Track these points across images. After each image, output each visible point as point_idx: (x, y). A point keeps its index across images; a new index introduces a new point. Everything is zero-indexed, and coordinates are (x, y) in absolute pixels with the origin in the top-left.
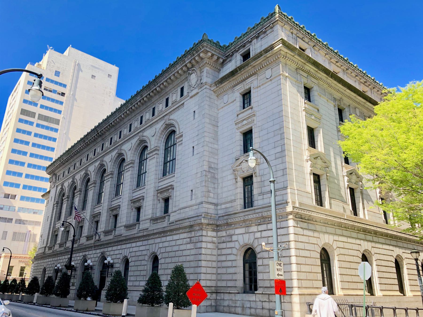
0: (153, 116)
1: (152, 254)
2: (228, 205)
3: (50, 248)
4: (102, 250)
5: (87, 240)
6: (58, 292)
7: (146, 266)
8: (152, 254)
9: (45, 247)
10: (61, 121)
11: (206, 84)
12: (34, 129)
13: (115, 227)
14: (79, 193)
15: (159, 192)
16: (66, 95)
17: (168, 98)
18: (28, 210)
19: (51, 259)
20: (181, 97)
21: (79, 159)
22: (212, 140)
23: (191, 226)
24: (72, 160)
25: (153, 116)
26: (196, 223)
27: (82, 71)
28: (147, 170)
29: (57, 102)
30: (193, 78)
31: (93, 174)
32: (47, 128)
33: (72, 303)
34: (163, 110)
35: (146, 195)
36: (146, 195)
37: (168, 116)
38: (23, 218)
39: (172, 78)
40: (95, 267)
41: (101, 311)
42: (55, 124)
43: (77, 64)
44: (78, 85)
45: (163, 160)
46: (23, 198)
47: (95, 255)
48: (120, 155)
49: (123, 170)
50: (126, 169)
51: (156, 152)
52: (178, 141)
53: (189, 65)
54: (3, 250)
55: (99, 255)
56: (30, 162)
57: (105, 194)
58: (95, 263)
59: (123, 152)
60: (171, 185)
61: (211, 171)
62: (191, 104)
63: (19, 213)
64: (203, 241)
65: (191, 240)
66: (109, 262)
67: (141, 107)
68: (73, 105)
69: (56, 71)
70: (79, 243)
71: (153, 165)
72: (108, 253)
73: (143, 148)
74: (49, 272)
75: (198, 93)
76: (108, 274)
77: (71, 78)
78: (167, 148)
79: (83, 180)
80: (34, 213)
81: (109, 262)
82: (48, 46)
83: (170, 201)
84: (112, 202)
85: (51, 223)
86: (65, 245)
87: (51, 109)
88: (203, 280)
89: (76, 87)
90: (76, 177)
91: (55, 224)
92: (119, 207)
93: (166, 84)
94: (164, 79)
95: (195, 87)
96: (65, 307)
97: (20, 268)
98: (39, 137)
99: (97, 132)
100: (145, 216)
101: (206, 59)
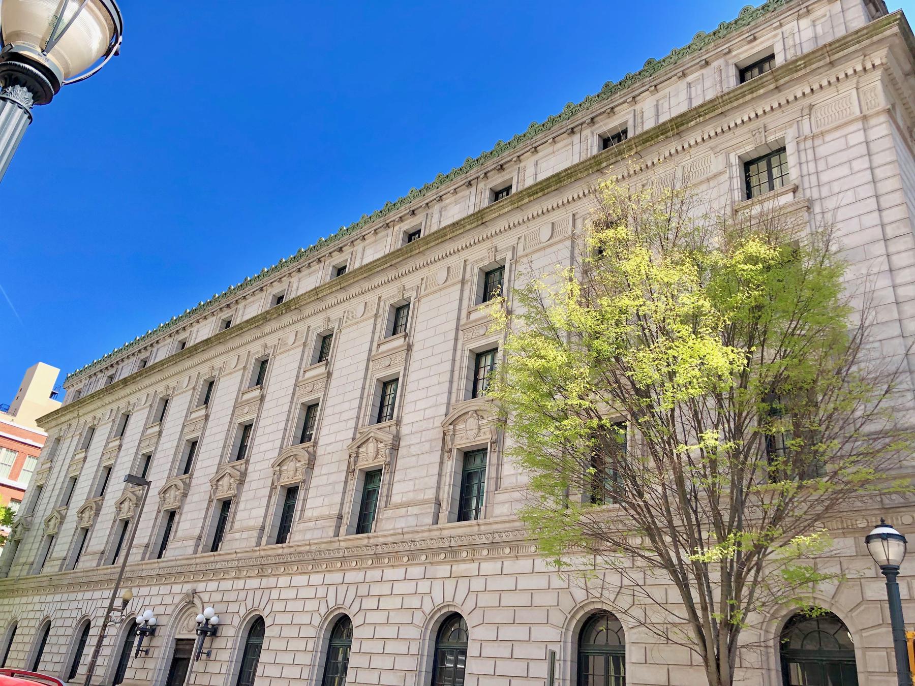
4: (188, 588)
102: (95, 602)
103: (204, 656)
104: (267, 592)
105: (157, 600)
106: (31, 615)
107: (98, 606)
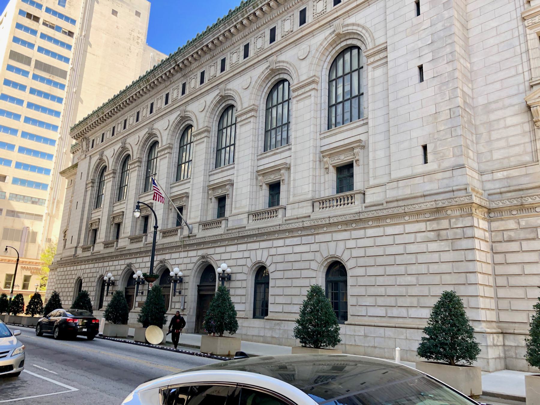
1: (255, 265)
2: (514, 173)
3: (85, 249)
4: (128, 261)
8: (326, 260)
9: (76, 247)
10: (68, 73)
12: (28, 82)
13: (117, 238)
15: (328, 155)
16: (75, 36)
17: (305, 9)
18: (24, 198)
20: (301, 24)
22: (463, 51)
23: (438, 210)
24: (119, 114)
26: (454, 203)
28: (157, 172)
29: (63, 44)
31: (135, 148)
32: (49, 82)
33: (131, 332)
35: (237, 179)
36: (237, 179)
37: (275, 56)
38: (17, 209)
39: (220, 39)
40: (186, 279)
46: (16, 181)
47: (186, 260)
48: (151, 135)
52: (239, 120)
54: (6, 249)
56: (26, 130)
58: (187, 273)
59: (155, 131)
60: (230, 180)
61: (467, 110)
63: (11, 202)
64: (476, 236)
65: (439, 235)
68: (85, 51)
70: (117, 246)
71: (201, 152)
72: (137, 266)
73: (185, 128)
77: (81, 10)
78: (222, 130)
79: (119, 156)
80: (33, 203)
81: (224, 271)
83: (228, 201)
87: (54, 55)
88: (482, 309)
91: (90, 214)
92: (187, 196)
96: (122, 338)
97: (23, 277)
98: (37, 95)
99: (176, 62)
105: (112, 268)
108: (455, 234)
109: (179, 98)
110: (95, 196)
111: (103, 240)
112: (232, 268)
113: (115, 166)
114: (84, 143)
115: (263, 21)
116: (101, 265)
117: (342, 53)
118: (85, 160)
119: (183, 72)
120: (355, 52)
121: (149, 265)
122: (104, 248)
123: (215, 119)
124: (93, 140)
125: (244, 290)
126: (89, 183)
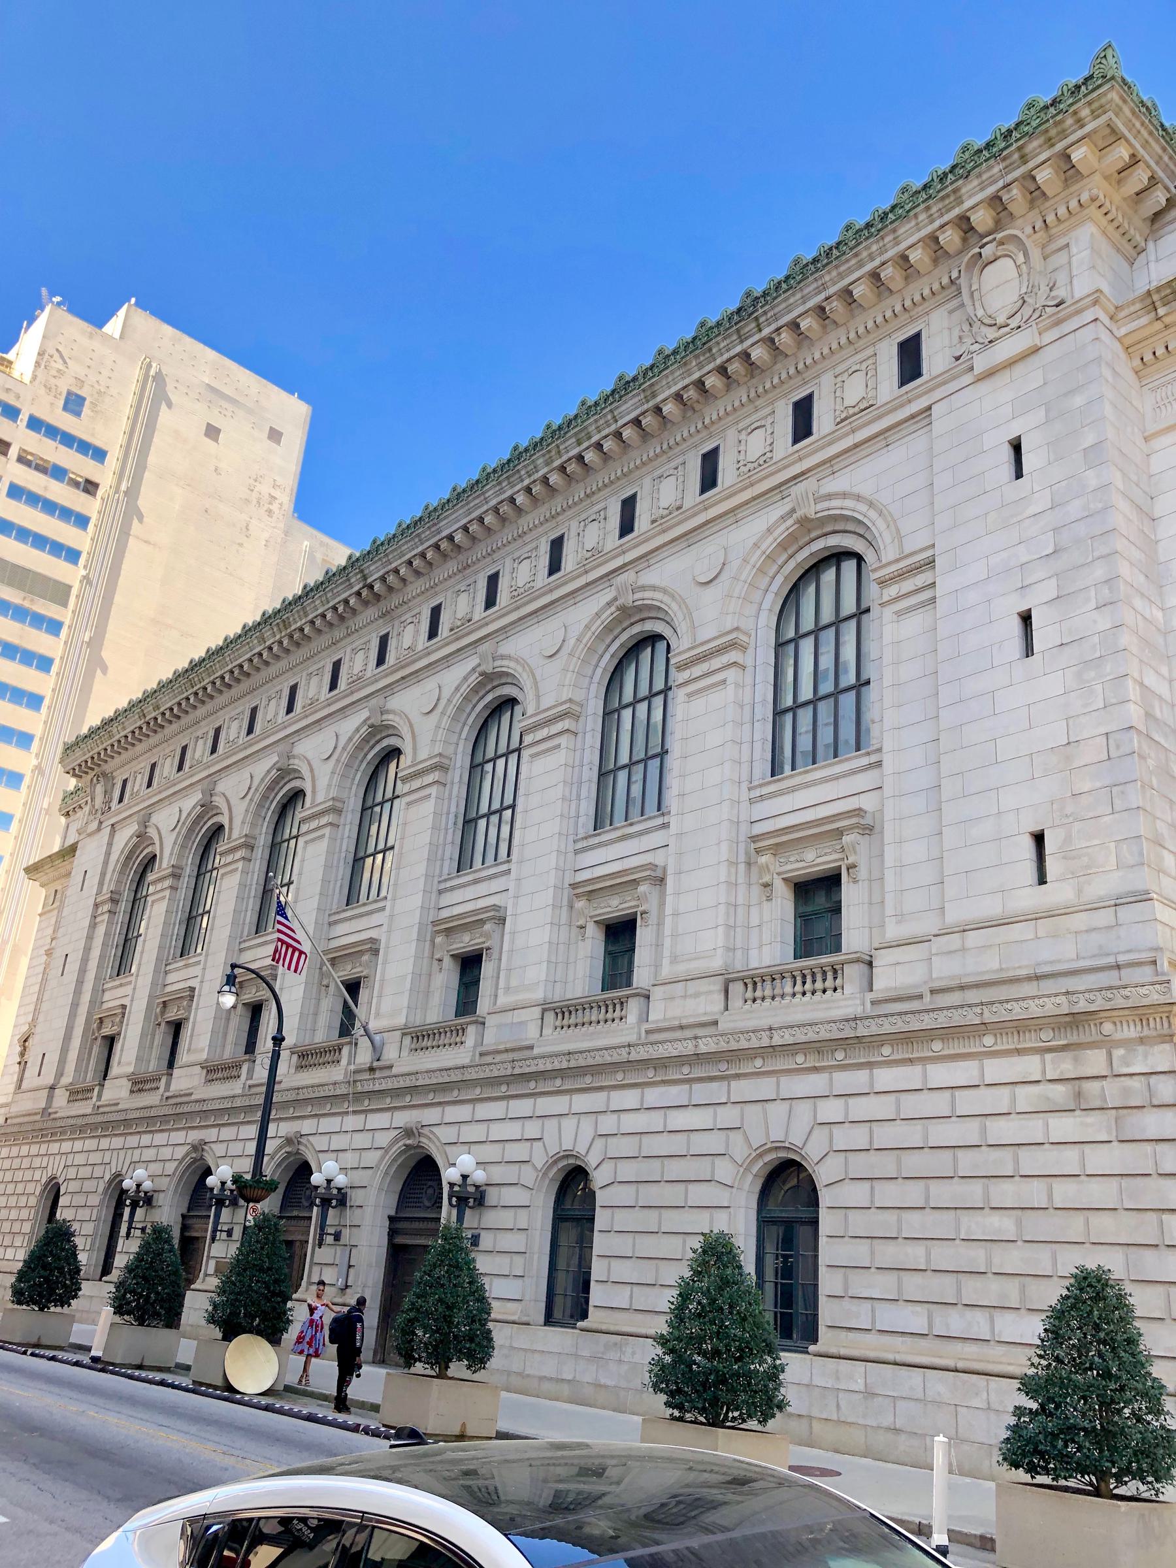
0: (331, 689)
3: (77, 1093)
4: (194, 1136)
5: (300, 1067)
6: (420, 1333)
7: (523, 1213)
8: (760, 1155)
9: (52, 1088)
10: (74, 592)
11: (1096, 302)
14: (167, 883)
15: (769, 848)
19: (91, 1144)
21: (245, 707)
22: (1142, 578)
23: (1075, 1020)
24: (201, 711)
25: (331, 689)
26: (1120, 1002)
27: (170, 405)
28: (869, 672)
29: (66, 514)
30: (1000, 284)
33: (185, 1350)
34: (369, 674)
35: (515, 905)
41: (375, 1408)
42: (53, 600)
43: (152, 373)
44: (152, 459)
45: (352, 849)
49: (216, 865)
50: (225, 865)
51: (733, 656)
52: (528, 739)
53: (982, 219)
55: (180, 1152)
57: (298, 889)
59: (296, 763)
60: (495, 908)
62: (977, 414)
65: (1079, 1095)
66: (465, 1177)
67: (634, 454)
69: (69, 393)
70: (167, 1088)
74: (79, 1200)
75: (1036, 350)
76: (215, 1231)
77: (124, 424)
79: (191, 830)
81: (465, 1177)
82: (44, 291)
83: (487, 969)
84: (440, 892)
85: (80, 982)
86: (168, 1085)
89: (141, 467)
90: (155, 819)
91: (99, 991)
93: (422, 564)
94: (804, 300)
95: (1014, 323)
96: (160, 1369)
99: (365, 578)
100: (674, 960)
101: (1097, 177)
102: (52, 1158)
103: (329, 1239)
104: (130, 1152)
106: (28, 1175)
107: (136, 1158)
108: (1126, 1092)
109: (369, 674)
110: (118, 939)
111: (131, 1069)
112: (156, 1179)
113: (180, 856)
114: (99, 789)
115: (602, 478)
116: (117, 1142)
117: (813, 570)
118: (97, 837)
119: (384, 605)
120: (849, 567)
121: (251, 1148)
122: (132, 1092)
123: (464, 736)
124: (125, 782)
125: (522, 1237)
126: (103, 903)
